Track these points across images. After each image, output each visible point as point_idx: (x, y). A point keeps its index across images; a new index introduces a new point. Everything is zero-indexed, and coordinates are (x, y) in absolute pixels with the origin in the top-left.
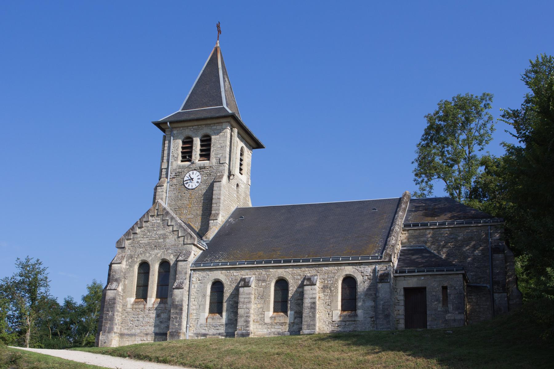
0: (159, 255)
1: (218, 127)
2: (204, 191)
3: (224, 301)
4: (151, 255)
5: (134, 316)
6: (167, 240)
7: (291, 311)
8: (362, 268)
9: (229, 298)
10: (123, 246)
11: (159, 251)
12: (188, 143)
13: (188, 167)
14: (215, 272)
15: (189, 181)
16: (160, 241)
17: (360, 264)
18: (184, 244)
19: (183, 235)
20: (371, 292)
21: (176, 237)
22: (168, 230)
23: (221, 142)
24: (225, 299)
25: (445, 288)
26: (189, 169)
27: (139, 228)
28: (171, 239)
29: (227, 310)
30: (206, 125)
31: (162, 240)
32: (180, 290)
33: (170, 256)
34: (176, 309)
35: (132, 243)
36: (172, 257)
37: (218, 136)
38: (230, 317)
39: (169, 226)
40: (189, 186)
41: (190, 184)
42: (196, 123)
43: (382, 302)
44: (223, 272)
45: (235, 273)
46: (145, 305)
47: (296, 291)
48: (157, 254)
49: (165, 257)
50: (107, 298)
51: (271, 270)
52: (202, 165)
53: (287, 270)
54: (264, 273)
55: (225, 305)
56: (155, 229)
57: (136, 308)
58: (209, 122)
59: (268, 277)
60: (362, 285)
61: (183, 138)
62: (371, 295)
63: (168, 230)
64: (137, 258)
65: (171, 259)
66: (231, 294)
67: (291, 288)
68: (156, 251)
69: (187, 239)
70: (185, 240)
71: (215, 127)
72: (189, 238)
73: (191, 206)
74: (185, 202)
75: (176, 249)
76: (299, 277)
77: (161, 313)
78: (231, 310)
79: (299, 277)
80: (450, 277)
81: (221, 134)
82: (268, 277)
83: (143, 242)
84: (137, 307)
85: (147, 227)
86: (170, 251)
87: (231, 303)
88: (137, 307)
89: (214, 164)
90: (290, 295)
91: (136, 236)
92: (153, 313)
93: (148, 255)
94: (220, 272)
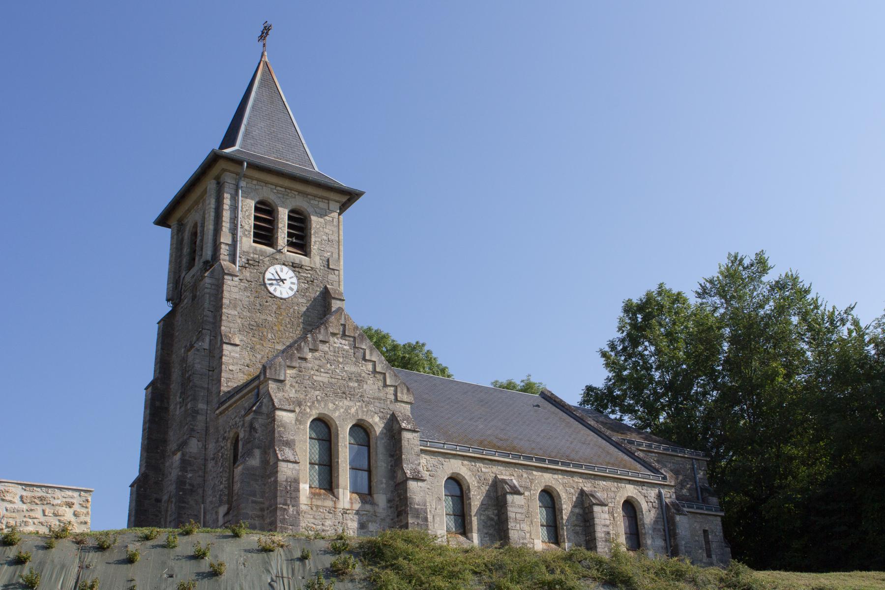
0: (353, 410)
1: (323, 205)
2: (304, 309)
3: (473, 513)
4: (337, 408)
5: (316, 522)
6: (365, 386)
7: (569, 541)
8: (645, 490)
9: (479, 509)
10: (282, 378)
11: (351, 404)
12: (265, 214)
13: (271, 256)
14: (452, 461)
15: (274, 282)
16: (351, 384)
17: (642, 484)
18: (396, 400)
19: (394, 384)
20: (659, 527)
21: (381, 384)
22: (364, 368)
23: (327, 231)
24: (474, 509)
25: (705, 532)
26: (274, 261)
27: (311, 350)
28: (371, 386)
29: (479, 530)
30: (300, 192)
31: (356, 384)
32: (420, 484)
33: (372, 417)
34: (418, 517)
35: (298, 376)
36: (377, 419)
37: (321, 220)
38: (87, 539)
39: (364, 359)
40: (275, 290)
41: (278, 287)
42: (287, 183)
43: (683, 542)
44: (466, 462)
45: (485, 468)
46: (335, 503)
47: (572, 512)
48: (349, 407)
49: (364, 418)
50: (281, 477)
51: (535, 473)
52: (297, 261)
53: (556, 476)
54: (525, 475)
55: (475, 520)
56: (341, 360)
57: (317, 507)
58: (310, 190)
59: (531, 483)
60: (649, 515)
61: (257, 200)
62: (659, 530)
63: (364, 368)
64: (310, 407)
65: (376, 424)
66: (482, 504)
67: (564, 506)
68: (347, 403)
69: (402, 393)
70: (399, 395)
71: (316, 203)
72: (405, 391)
73: (282, 328)
74: (270, 318)
75: (382, 405)
76: (572, 491)
77: (369, 521)
78: (485, 531)
79: (572, 491)
80: (710, 518)
81: (327, 218)
82: (531, 483)
83: (319, 378)
84: (319, 503)
85: (325, 353)
86: (371, 408)
87: (483, 518)
88: (319, 503)
89: (318, 266)
90: (565, 517)
91: (304, 364)
92: (352, 520)
93: (331, 405)
94: (460, 462)
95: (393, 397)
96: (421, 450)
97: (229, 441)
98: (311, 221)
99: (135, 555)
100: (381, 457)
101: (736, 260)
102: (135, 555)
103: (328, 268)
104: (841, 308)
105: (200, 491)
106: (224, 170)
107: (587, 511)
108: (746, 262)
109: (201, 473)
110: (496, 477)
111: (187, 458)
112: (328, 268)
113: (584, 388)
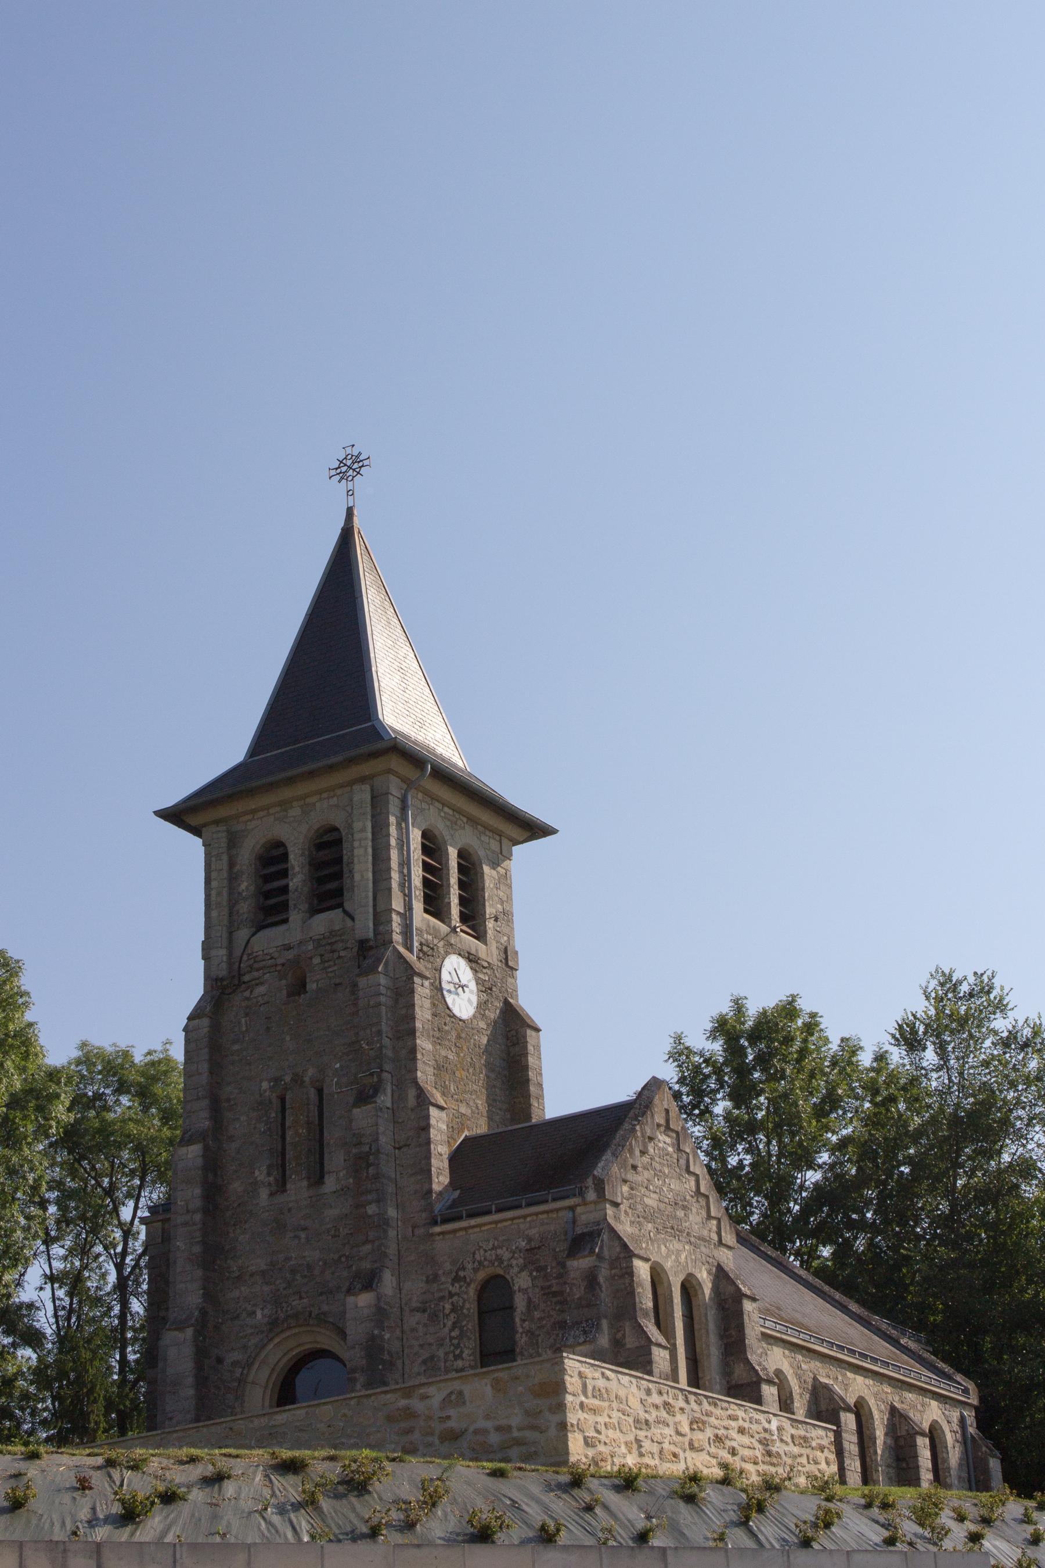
21: (704, 1213)
36: (705, 1274)
58: (485, 816)
95: (715, 1237)
96: (763, 1334)
97: (473, 1286)
98: (483, 873)
99: (507, 1477)
100: (713, 1338)
101: (948, 983)
102: (507, 1477)
103: (507, 964)
104: (903, 1013)
105: (399, 1363)
106: (390, 771)
107: (902, 1442)
108: (964, 988)
109: (398, 1332)
110: (815, 1379)
111: (382, 1304)
112: (507, 964)
113: (123, 1045)
